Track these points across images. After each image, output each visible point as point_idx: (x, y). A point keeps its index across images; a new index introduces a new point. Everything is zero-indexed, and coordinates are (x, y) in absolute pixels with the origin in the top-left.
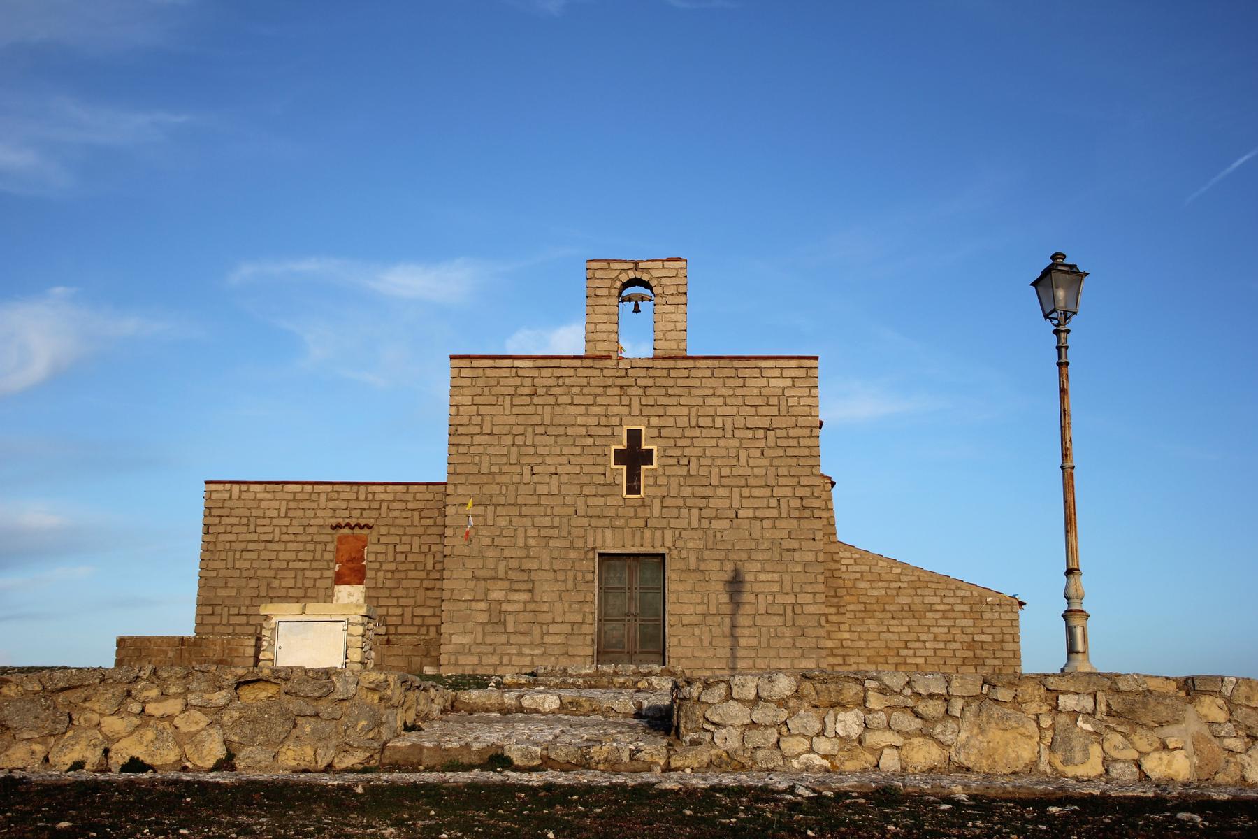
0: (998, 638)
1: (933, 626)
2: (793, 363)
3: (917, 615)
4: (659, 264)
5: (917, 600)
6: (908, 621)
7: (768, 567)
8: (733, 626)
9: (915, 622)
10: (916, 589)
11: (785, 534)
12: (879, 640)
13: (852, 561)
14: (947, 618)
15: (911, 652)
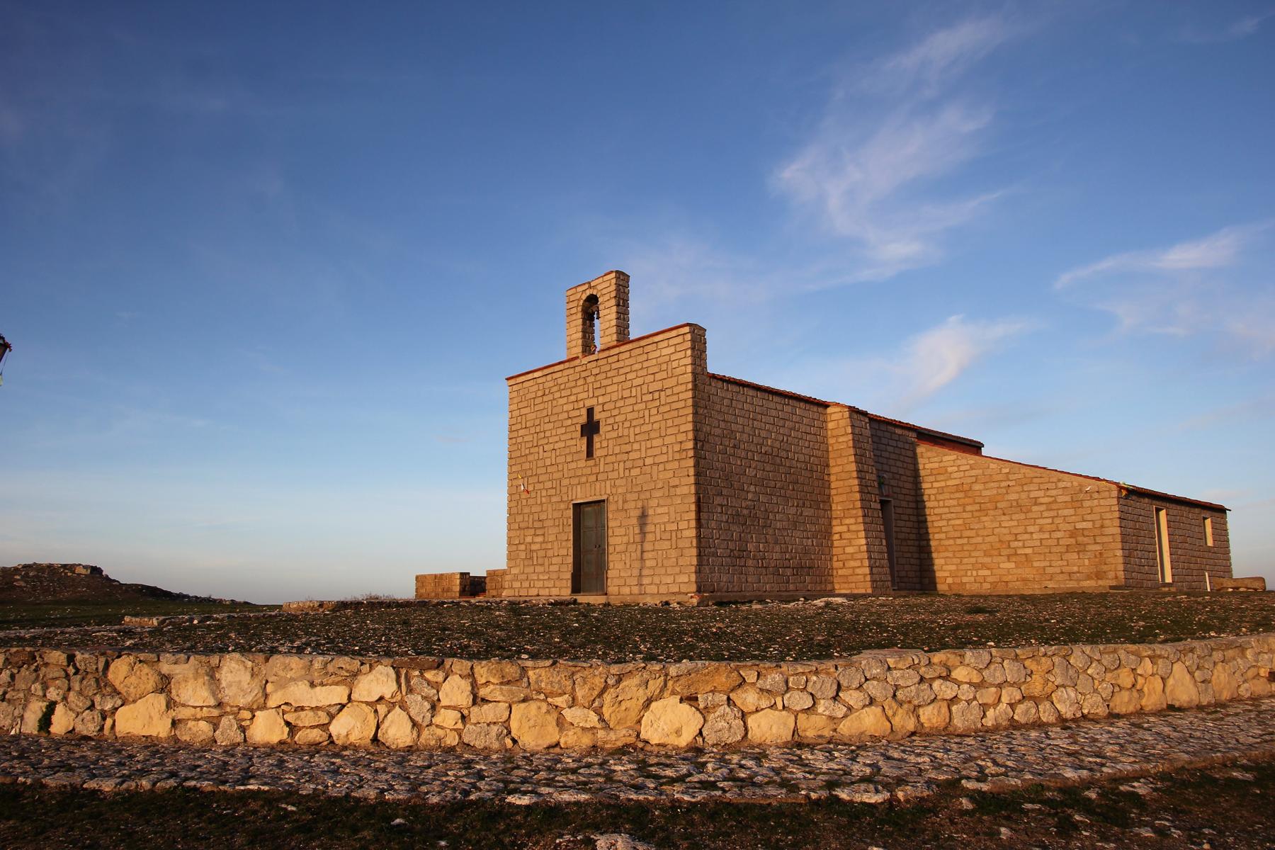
0: (1098, 524)
1: (1038, 518)
2: (674, 333)
3: (1024, 510)
4: (601, 280)
5: (1024, 496)
6: (1017, 515)
7: (662, 502)
8: (642, 552)
9: (1022, 516)
10: (1022, 485)
11: (670, 474)
12: (994, 534)
13: (968, 467)
14: (1051, 510)
15: (1020, 544)
